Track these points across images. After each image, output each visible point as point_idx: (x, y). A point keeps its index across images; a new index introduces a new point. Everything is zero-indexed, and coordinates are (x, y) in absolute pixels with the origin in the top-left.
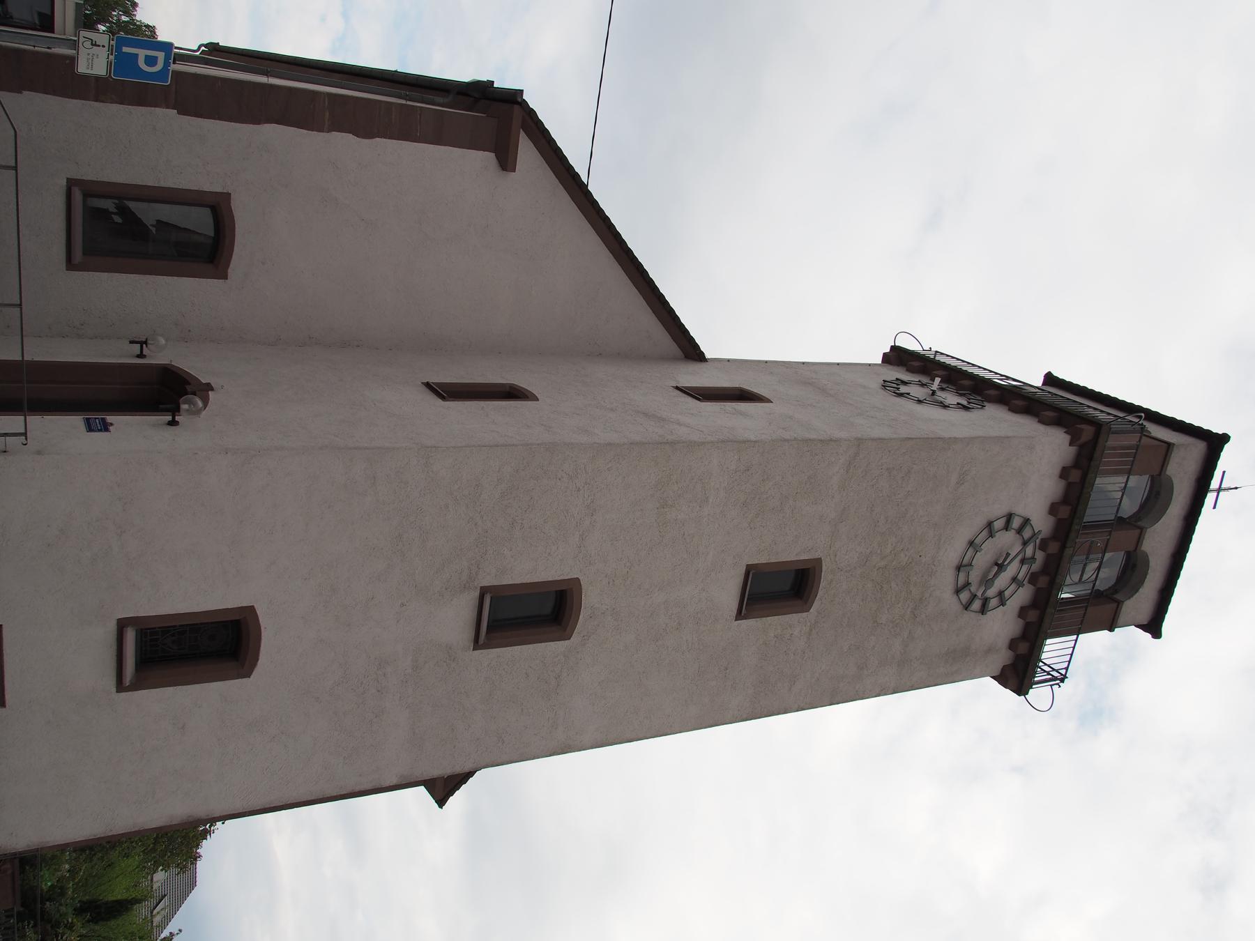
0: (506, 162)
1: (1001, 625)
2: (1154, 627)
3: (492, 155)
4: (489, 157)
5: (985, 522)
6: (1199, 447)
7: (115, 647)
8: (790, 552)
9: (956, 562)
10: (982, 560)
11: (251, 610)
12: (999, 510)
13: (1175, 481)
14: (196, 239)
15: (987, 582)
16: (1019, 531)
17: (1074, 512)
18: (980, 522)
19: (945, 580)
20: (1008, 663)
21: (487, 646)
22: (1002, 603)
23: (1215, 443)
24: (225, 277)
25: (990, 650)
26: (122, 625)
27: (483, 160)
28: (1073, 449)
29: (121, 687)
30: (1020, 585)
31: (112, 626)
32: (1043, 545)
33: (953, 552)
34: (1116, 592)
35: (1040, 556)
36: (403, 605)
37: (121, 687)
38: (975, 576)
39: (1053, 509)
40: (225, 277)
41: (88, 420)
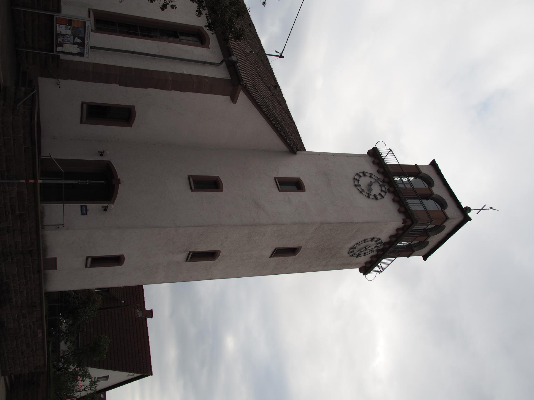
0: (234, 99)
1: (363, 260)
2: (425, 258)
3: (229, 97)
4: (228, 98)
14: (124, 116)
17: (403, 233)
21: (190, 261)
26: (87, 258)
27: (225, 99)
28: (403, 225)
31: (85, 258)
34: (430, 231)
41: (82, 206)
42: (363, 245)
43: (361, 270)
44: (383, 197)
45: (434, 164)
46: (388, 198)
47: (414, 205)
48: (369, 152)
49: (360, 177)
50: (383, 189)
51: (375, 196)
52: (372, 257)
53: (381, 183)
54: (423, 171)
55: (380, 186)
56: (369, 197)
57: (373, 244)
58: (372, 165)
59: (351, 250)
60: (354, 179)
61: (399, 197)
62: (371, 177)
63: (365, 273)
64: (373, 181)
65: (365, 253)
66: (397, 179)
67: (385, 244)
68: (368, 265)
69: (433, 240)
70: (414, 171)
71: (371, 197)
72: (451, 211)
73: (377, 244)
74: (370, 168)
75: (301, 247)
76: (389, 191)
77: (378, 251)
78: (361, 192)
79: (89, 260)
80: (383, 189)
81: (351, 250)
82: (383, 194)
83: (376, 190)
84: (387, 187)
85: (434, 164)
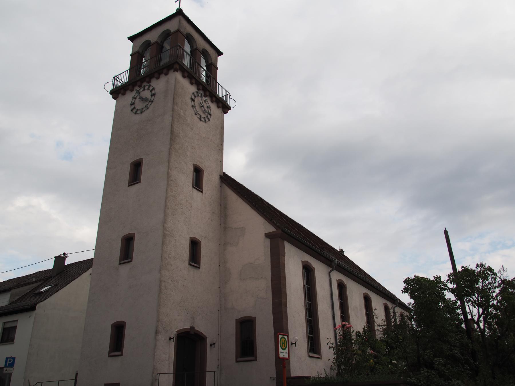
1: (213, 108)
21: (199, 264)
31: (309, 358)
42: (198, 108)
43: (226, 112)
44: (154, 88)
45: (132, 39)
46: (154, 83)
47: (165, 60)
48: (114, 98)
49: (134, 108)
50: (147, 87)
51: (152, 96)
52: (212, 101)
53: (142, 89)
54: (137, 49)
55: (144, 90)
56: (152, 102)
57: (198, 100)
58: (159, 80)
59: (203, 120)
60: (136, 113)
61: (159, 71)
62: (136, 98)
63: (229, 108)
64: (138, 97)
65: (208, 108)
66: (143, 72)
67: (198, 89)
68: (220, 105)
69: (201, 44)
70: (136, 58)
71: (152, 99)
72: (172, 26)
73: (198, 96)
74: (129, 97)
75: (194, 165)
76: (149, 82)
77: (206, 96)
78: (148, 108)
79: (311, 355)
80: (147, 87)
81: (203, 120)
82: (151, 88)
83: (146, 94)
84: (145, 84)
85: (132, 39)
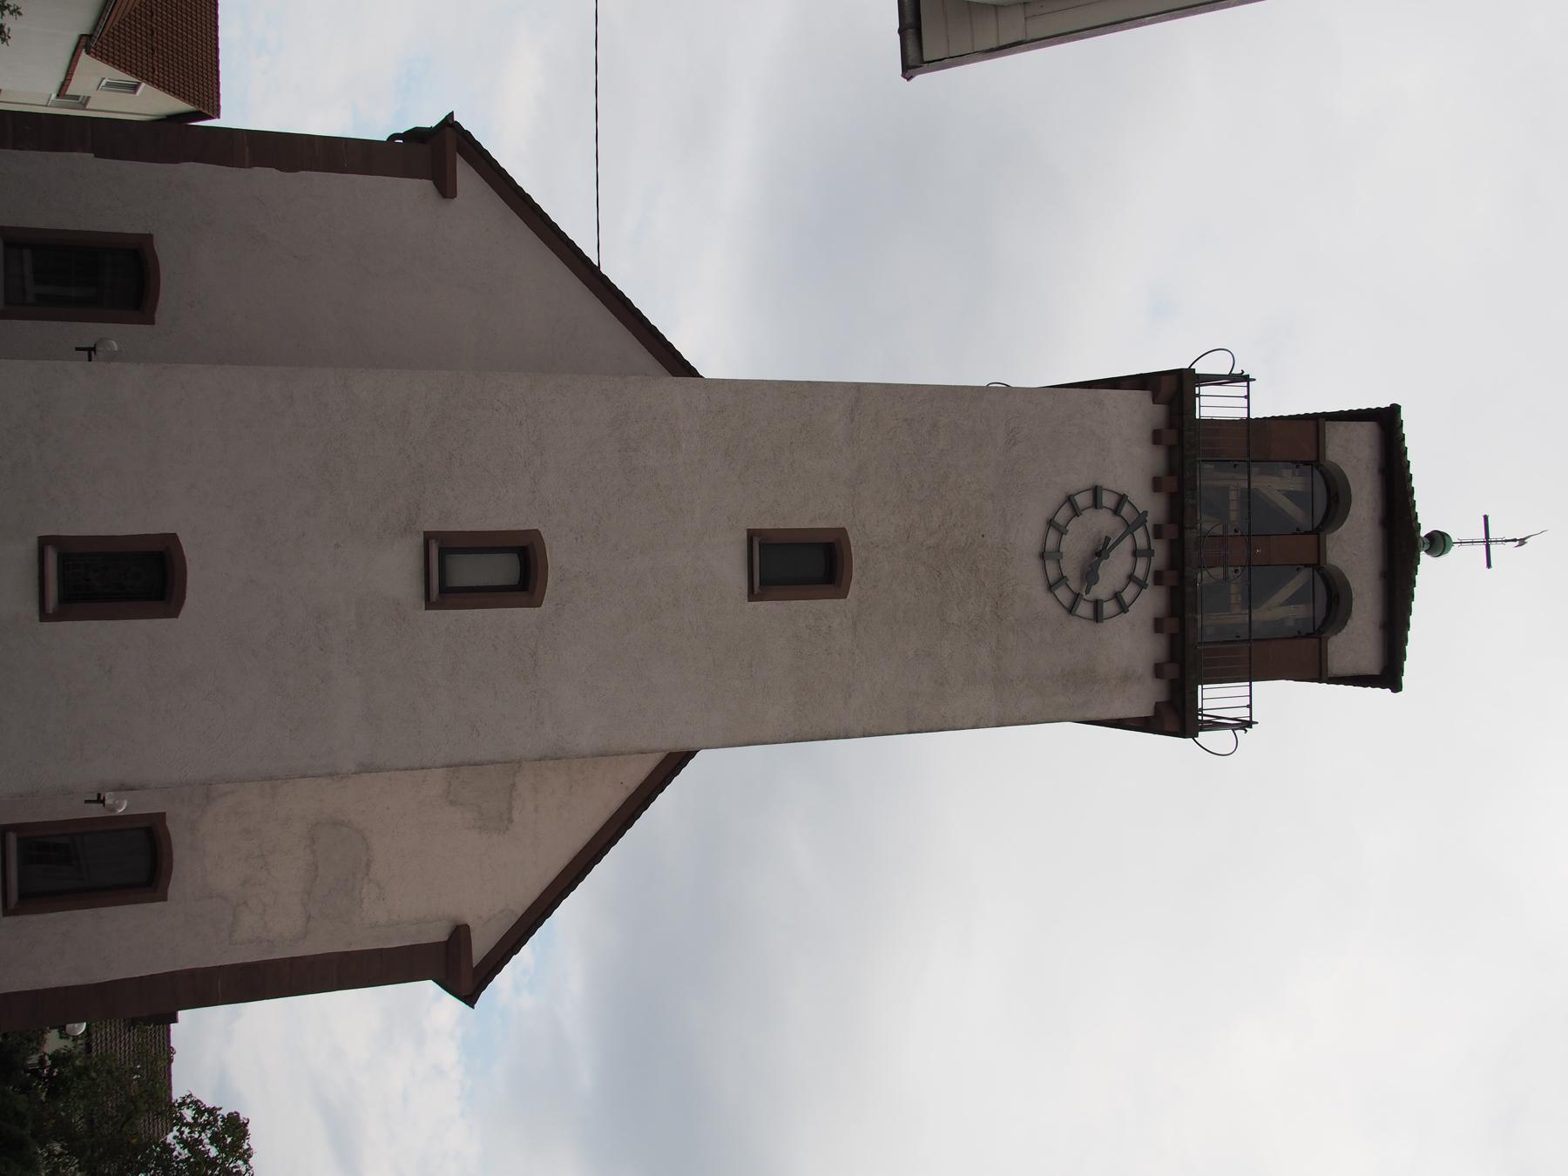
0: (446, 189)
1: (1131, 642)
4: (427, 185)
5: (1062, 497)
6: (1368, 429)
7: (36, 568)
8: (801, 514)
9: (1037, 549)
10: (1076, 545)
11: (174, 537)
12: (1078, 480)
13: (1348, 471)
15: (1090, 575)
16: (1116, 511)
18: (1057, 496)
19: (1030, 576)
20: (1162, 698)
22: (1123, 608)
23: (1387, 421)
24: (152, 322)
25: (1126, 678)
26: (44, 542)
29: (44, 616)
30: (1142, 585)
31: (33, 543)
32: (1158, 532)
33: (1028, 535)
35: (1160, 548)
36: (337, 546)
37: (44, 616)
38: (1071, 568)
39: (1156, 485)
40: (152, 322)
